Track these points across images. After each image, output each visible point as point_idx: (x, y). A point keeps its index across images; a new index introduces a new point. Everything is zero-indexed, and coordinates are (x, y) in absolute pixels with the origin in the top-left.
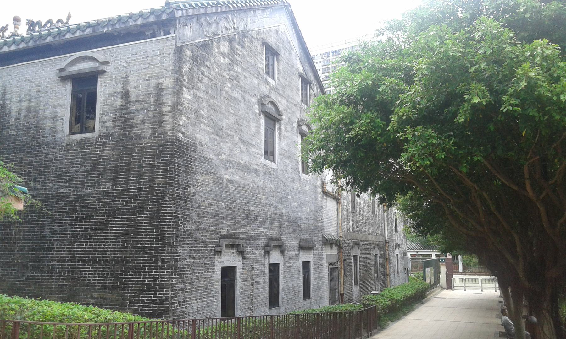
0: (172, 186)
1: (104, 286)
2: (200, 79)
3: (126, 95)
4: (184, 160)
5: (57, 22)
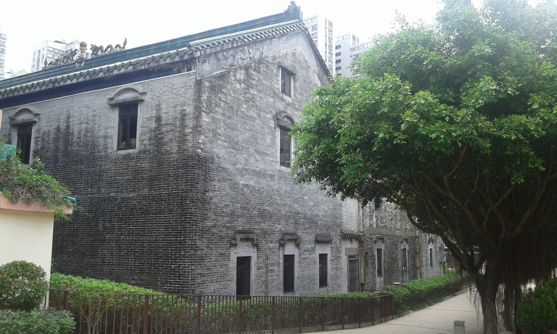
0: (192, 192)
1: (142, 270)
2: (218, 104)
3: (158, 119)
4: (203, 170)
5: (116, 47)
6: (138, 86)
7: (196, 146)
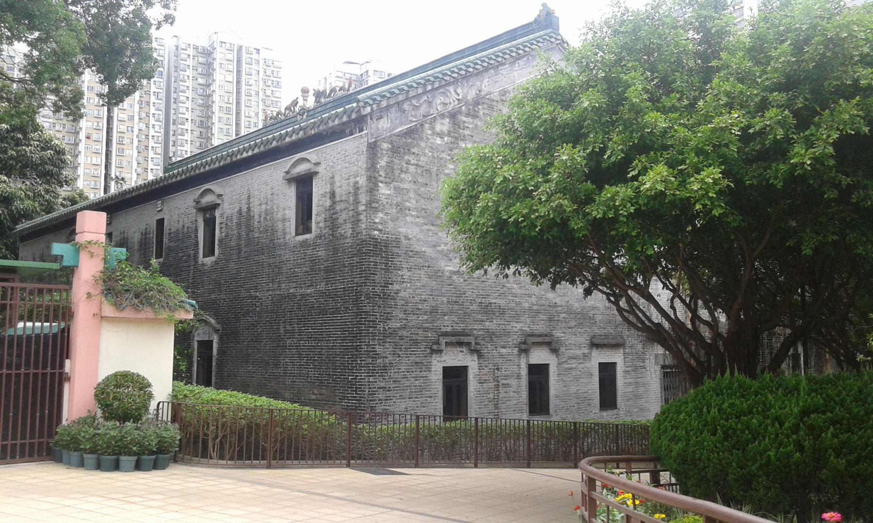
3: (333, 195)
6: (311, 154)
7: (372, 226)
